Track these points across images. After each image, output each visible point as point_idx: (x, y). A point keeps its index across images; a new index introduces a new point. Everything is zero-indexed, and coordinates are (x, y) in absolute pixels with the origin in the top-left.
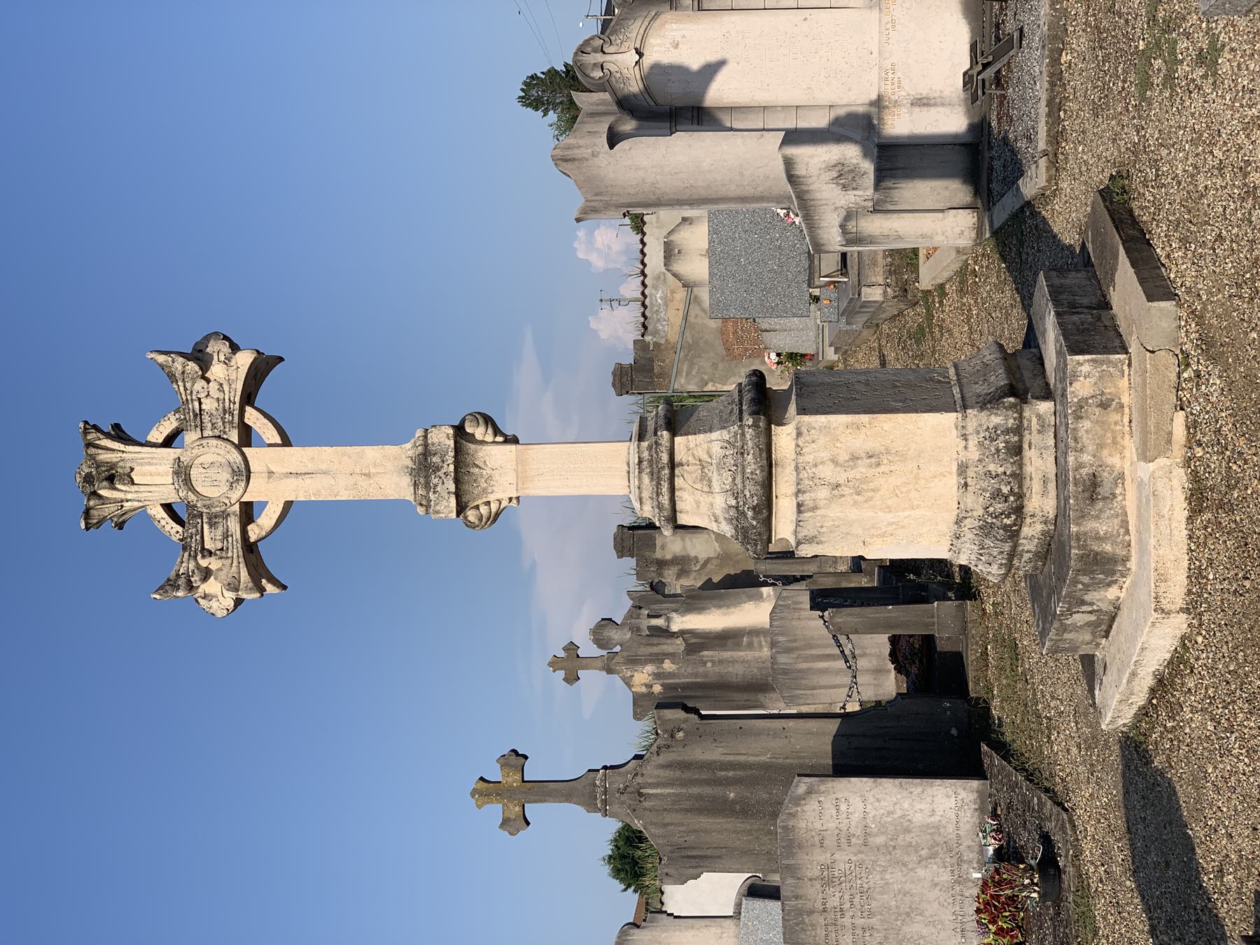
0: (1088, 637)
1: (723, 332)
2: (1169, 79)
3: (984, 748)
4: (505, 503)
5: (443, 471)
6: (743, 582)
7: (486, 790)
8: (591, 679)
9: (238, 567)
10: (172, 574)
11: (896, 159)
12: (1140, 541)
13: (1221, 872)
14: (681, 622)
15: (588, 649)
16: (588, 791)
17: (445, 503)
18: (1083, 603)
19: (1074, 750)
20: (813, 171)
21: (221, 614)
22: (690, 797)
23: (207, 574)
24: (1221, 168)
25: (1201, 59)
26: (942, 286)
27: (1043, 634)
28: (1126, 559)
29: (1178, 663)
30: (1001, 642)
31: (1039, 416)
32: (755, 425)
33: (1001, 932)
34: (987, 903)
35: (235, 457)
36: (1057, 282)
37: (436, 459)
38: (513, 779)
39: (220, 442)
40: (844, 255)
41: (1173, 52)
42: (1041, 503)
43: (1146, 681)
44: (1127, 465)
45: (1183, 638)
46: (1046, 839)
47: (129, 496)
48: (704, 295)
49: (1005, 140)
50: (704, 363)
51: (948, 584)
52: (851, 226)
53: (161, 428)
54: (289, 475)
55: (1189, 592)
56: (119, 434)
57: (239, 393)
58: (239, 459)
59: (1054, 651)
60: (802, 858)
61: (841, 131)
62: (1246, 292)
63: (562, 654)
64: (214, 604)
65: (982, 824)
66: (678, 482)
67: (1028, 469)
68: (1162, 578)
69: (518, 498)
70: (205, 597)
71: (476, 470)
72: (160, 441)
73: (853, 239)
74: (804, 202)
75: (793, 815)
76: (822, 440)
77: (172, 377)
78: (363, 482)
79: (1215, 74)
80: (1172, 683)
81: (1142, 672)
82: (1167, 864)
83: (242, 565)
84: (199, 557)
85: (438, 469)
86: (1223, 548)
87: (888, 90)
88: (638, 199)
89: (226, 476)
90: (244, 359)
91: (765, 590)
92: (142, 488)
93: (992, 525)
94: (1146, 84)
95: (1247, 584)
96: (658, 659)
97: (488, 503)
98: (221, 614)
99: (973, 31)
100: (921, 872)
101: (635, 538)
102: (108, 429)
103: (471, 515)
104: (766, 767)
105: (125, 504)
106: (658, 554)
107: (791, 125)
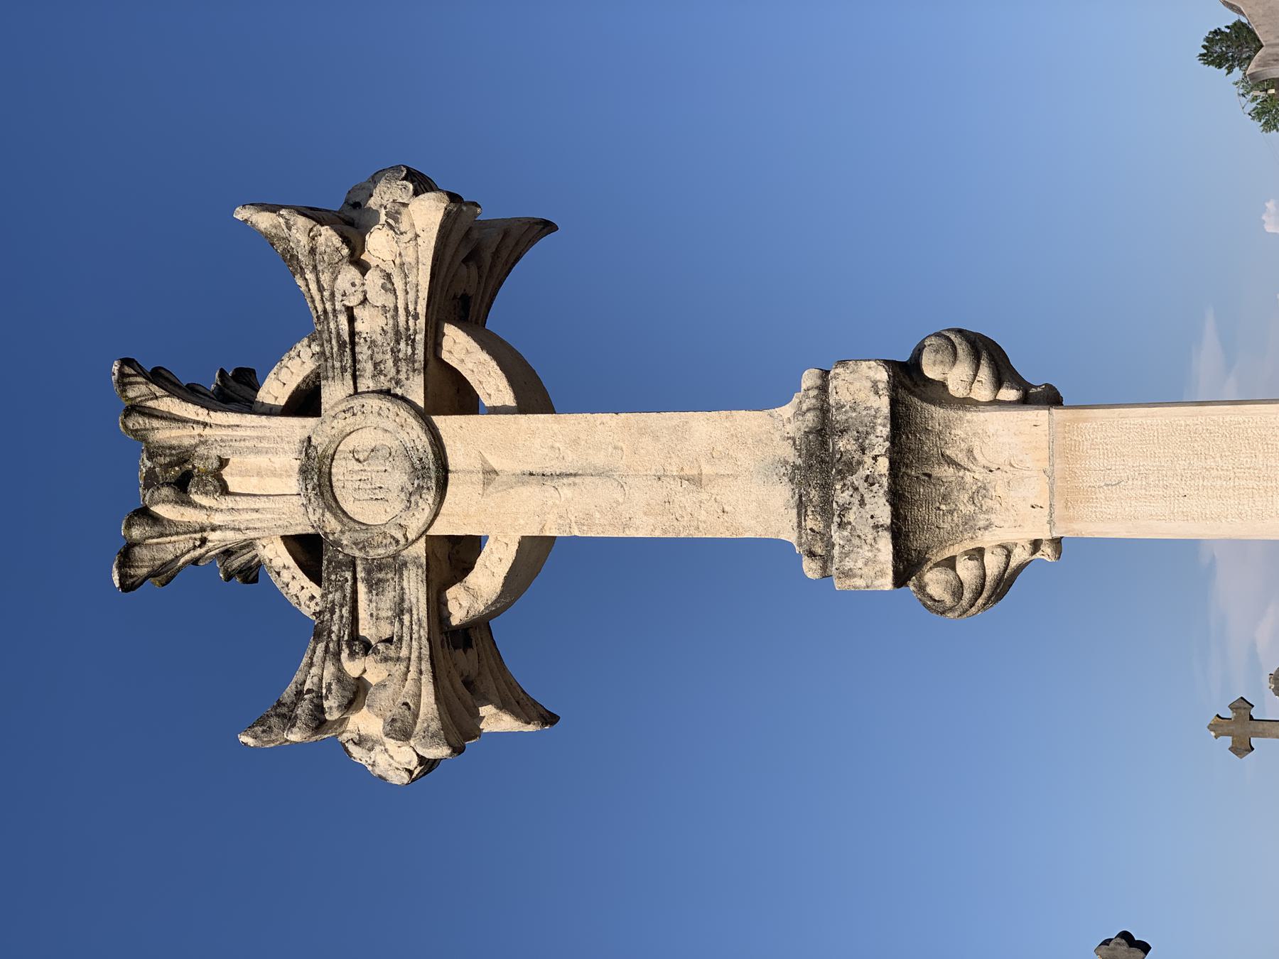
4: (1020, 556)
5: (863, 472)
9: (418, 681)
10: (289, 693)
17: (866, 552)
23: (356, 693)
35: (416, 435)
37: (844, 444)
39: (386, 404)
47: (217, 519)
53: (284, 374)
54: (534, 478)
57: (424, 294)
63: (1229, 714)
69: (1057, 542)
70: (360, 741)
71: (947, 472)
72: (282, 402)
78: (685, 498)
83: (427, 679)
84: (344, 655)
85: (851, 467)
89: (398, 478)
92: (242, 503)
97: (977, 554)
103: (935, 582)
105: (212, 536)
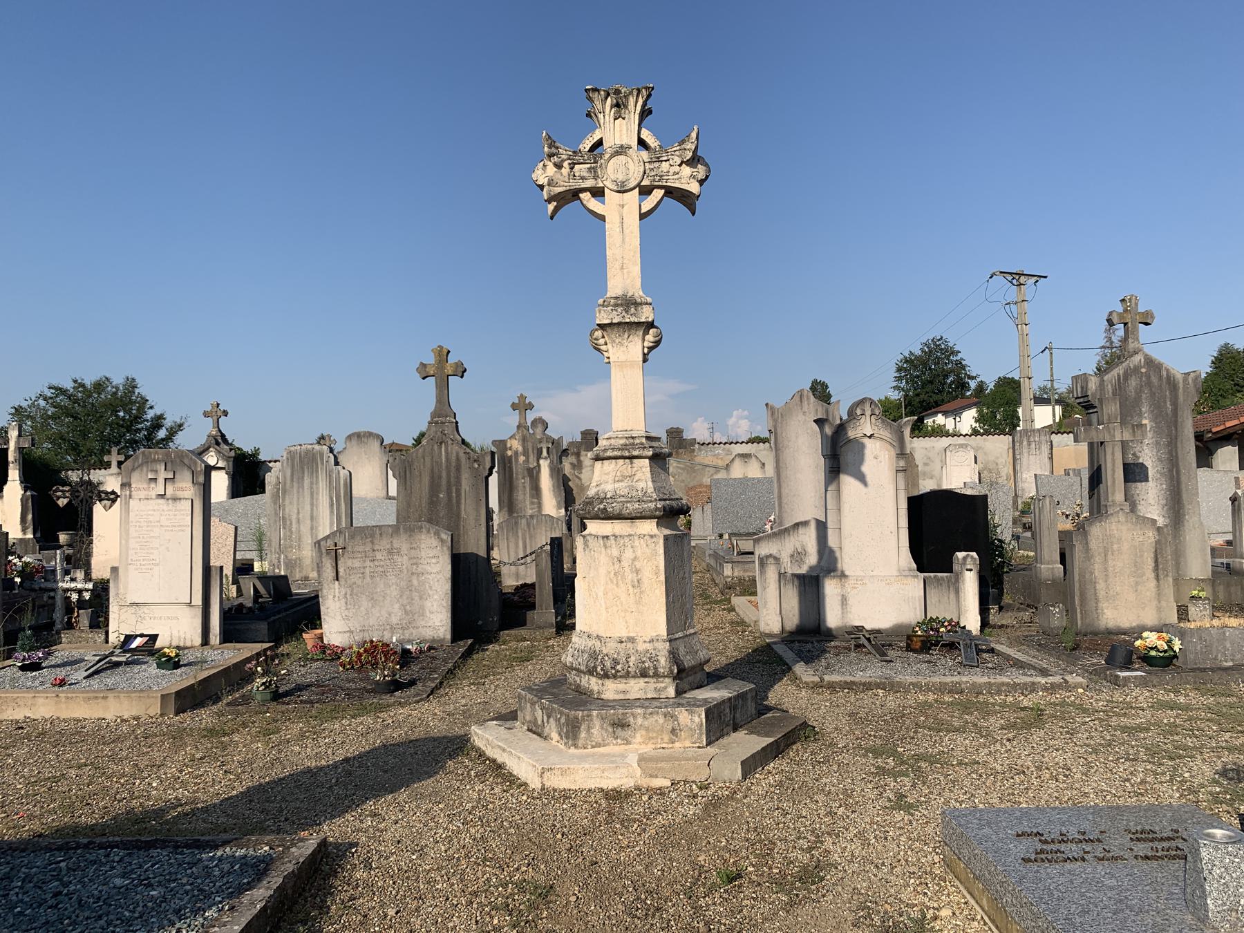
0: (528, 718)
1: (701, 485)
2: (882, 772)
3: (470, 641)
6: (568, 496)
7: (443, 355)
8: (514, 419)
11: (810, 586)
12: (588, 756)
13: (374, 815)
14: (545, 465)
15: (531, 416)
16: (443, 413)
18: (549, 717)
19: (463, 702)
20: (801, 538)
21: (534, 176)
22: (440, 472)
23: (559, 166)
24: (831, 813)
25: (900, 797)
26: (733, 610)
27: (529, 689)
28: (576, 746)
29: (511, 780)
30: (531, 650)
31: (665, 688)
32: (657, 509)
33: (359, 655)
34: (376, 647)
35: (633, 183)
36: (749, 696)
38: (449, 370)
40: (752, 553)
41: (901, 774)
42: (611, 690)
43: (500, 758)
44: (635, 746)
45: (526, 784)
46: (412, 683)
48: (722, 475)
49: (824, 651)
50: (684, 476)
51: (564, 617)
52: (771, 560)
54: (621, 217)
55: (555, 790)
56: (645, 113)
58: (631, 186)
59: (520, 696)
60: (404, 537)
61: (825, 557)
62: (752, 836)
64: (540, 172)
65: (424, 641)
66: (621, 461)
67: (632, 682)
68: (564, 772)
73: (763, 562)
74: (782, 533)
75: (428, 532)
76: (648, 551)
77: (683, 142)
78: (618, 265)
79: (892, 808)
80: (498, 776)
81: (505, 755)
82: (386, 772)
86: (583, 817)
87: (851, 581)
88: (780, 439)
89: (621, 178)
90: (694, 188)
91: (563, 511)
93: (596, 659)
94: (877, 753)
95: (559, 836)
96: (526, 453)
98: (534, 176)
99: (886, 630)
100: (397, 606)
101: (590, 438)
102: (648, 106)
103: (598, 333)
104: (458, 515)
106: (583, 453)
107: (830, 525)
